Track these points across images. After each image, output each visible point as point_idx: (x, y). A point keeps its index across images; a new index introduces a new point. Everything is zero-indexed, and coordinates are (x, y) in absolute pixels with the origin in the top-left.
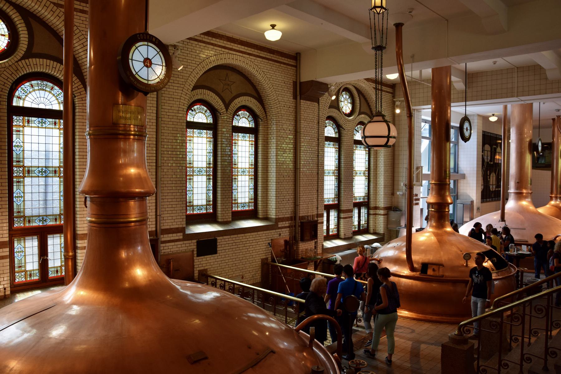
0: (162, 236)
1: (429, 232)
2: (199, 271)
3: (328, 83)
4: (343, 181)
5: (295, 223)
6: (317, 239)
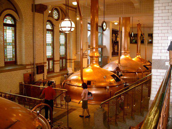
1: (90, 68)
3: (47, 5)
4: (55, 48)
6: (44, 73)
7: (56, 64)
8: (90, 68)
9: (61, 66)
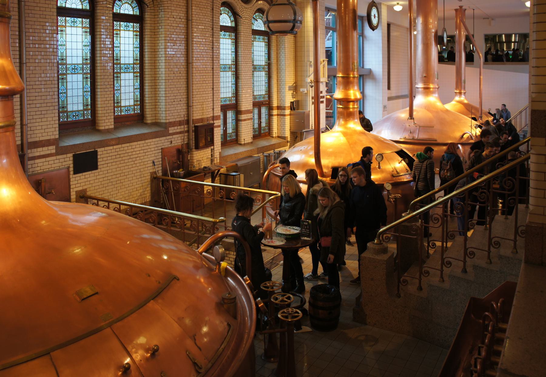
0: (29, 151)
1: (338, 132)
2: (76, 192)
5: (188, 127)
7: (245, 120)
8: (338, 132)
9: (256, 126)
